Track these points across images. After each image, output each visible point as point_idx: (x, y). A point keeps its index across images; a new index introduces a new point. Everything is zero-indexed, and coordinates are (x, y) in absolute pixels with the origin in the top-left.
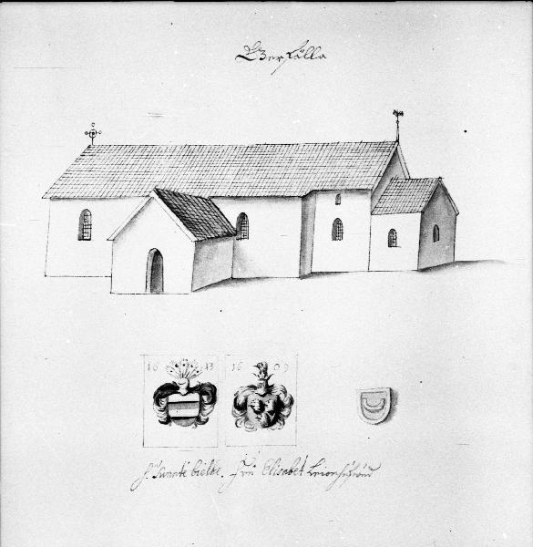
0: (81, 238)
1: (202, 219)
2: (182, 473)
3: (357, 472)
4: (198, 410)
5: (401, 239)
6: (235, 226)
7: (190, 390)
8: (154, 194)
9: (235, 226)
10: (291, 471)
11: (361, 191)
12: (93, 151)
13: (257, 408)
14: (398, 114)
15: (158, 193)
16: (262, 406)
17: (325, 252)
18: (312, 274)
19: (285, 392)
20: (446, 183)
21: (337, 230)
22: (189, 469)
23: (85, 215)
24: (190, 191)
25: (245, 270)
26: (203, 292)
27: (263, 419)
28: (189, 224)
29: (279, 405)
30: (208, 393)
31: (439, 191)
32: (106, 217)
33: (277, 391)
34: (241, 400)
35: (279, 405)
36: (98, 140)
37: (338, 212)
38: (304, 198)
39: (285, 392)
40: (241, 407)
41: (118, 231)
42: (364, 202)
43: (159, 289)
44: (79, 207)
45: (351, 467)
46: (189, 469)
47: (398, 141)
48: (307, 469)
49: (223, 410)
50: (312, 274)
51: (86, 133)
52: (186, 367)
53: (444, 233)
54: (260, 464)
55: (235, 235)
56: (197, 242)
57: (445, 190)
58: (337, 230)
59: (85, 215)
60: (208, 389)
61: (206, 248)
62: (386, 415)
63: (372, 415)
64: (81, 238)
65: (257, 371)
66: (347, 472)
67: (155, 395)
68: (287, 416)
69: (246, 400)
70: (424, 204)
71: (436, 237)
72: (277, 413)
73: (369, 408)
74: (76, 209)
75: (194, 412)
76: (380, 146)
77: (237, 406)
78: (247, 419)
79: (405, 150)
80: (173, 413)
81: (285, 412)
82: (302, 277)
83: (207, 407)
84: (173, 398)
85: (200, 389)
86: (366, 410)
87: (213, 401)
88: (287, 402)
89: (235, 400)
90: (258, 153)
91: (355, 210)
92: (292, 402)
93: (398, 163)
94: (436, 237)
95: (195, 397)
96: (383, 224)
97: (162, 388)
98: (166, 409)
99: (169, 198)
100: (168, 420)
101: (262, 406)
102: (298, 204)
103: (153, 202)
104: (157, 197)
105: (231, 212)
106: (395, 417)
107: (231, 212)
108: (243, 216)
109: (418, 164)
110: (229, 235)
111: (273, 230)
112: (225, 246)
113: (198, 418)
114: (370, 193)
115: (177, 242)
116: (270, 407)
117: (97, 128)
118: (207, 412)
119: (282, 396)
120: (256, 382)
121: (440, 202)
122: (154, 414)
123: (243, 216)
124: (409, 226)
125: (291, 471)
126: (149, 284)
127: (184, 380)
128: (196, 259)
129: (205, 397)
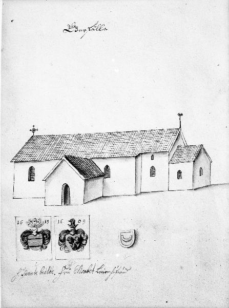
3: (120, 271)
4: (42, 242)
6: (103, 171)
8: (64, 158)
9: (103, 171)
10: (88, 271)
14: (180, 115)
19: (84, 233)
21: (153, 172)
23: (31, 169)
26: (94, 202)
28: (82, 172)
29: (81, 240)
32: (42, 169)
35: (81, 240)
36: (36, 133)
37: (152, 163)
38: (136, 157)
41: (48, 176)
43: (68, 201)
45: (116, 269)
46: (39, 270)
51: (30, 130)
52: (36, 222)
53: (205, 172)
54: (73, 270)
55: (103, 176)
56: (85, 180)
57: (204, 149)
58: (153, 172)
59: (31, 169)
60: (46, 233)
61: (90, 183)
62: (133, 241)
63: (123, 242)
65: (70, 223)
66: (115, 271)
67: (21, 236)
68: (85, 245)
69: (65, 237)
70: (194, 158)
73: (125, 240)
77: (60, 240)
78: (66, 246)
79: (184, 131)
81: (84, 242)
82: (136, 195)
84: (30, 237)
85: (43, 233)
86: (123, 240)
89: (60, 238)
90: (113, 136)
91: (161, 162)
92: (87, 238)
93: (181, 138)
96: (175, 168)
97: (25, 233)
100: (28, 248)
102: (134, 158)
103: (64, 162)
104: (65, 159)
106: (139, 242)
108: (107, 166)
110: (100, 176)
111: (121, 170)
112: (100, 180)
114: (168, 153)
115: (76, 180)
117: (36, 128)
118: (47, 243)
119: (82, 235)
121: (202, 156)
123: (107, 166)
125: (88, 271)
126: (63, 200)
127: (34, 229)
128: (85, 189)
129: (45, 236)
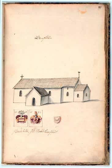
0: (20, 96)
1: (43, 93)
2: (21, 132)
5: (80, 96)
7: (23, 116)
8: (33, 88)
11: (72, 87)
12: (22, 80)
13: (35, 120)
15: (34, 88)
16: (36, 120)
17: (65, 98)
18: (63, 102)
20: (88, 85)
21: (68, 94)
22: (22, 131)
23: (21, 92)
24: (40, 87)
25: (50, 101)
27: (36, 122)
29: (39, 119)
30: (26, 117)
31: (87, 87)
32: (25, 92)
33: (39, 117)
34: (32, 119)
35: (39, 119)
36: (23, 78)
37: (68, 91)
38: (62, 88)
39: (40, 117)
40: (32, 120)
42: (72, 90)
44: (20, 90)
46: (22, 131)
47: (79, 77)
48: (44, 131)
49: (29, 121)
50: (63, 102)
57: (88, 87)
58: (68, 94)
59: (21, 92)
60: (25, 116)
61: (43, 98)
64: (20, 96)
71: (86, 96)
72: (39, 121)
74: (19, 90)
75: (23, 120)
76: (75, 78)
77: (31, 119)
79: (80, 79)
80: (19, 121)
82: (61, 103)
83: (26, 120)
84: (19, 118)
85: (24, 116)
86: (55, 120)
87: (27, 118)
88: (40, 119)
92: (41, 119)
94: (86, 96)
95: (23, 118)
96: (76, 93)
97: (18, 116)
98: (18, 120)
99: (36, 88)
100: (19, 122)
101: (36, 120)
102: (60, 89)
105: (48, 91)
106: (60, 123)
107: (48, 91)
108: (50, 91)
109: (83, 81)
111: (55, 95)
112: (47, 97)
113: (24, 121)
115: (38, 97)
116: (37, 119)
120: (35, 115)
121: (87, 89)
122: (16, 121)
123: (50, 91)
124: (81, 93)
